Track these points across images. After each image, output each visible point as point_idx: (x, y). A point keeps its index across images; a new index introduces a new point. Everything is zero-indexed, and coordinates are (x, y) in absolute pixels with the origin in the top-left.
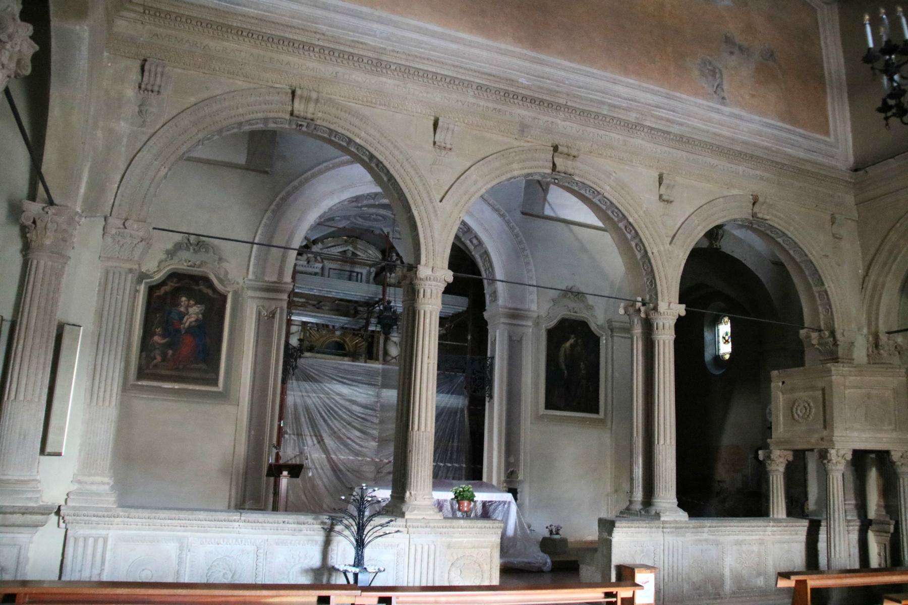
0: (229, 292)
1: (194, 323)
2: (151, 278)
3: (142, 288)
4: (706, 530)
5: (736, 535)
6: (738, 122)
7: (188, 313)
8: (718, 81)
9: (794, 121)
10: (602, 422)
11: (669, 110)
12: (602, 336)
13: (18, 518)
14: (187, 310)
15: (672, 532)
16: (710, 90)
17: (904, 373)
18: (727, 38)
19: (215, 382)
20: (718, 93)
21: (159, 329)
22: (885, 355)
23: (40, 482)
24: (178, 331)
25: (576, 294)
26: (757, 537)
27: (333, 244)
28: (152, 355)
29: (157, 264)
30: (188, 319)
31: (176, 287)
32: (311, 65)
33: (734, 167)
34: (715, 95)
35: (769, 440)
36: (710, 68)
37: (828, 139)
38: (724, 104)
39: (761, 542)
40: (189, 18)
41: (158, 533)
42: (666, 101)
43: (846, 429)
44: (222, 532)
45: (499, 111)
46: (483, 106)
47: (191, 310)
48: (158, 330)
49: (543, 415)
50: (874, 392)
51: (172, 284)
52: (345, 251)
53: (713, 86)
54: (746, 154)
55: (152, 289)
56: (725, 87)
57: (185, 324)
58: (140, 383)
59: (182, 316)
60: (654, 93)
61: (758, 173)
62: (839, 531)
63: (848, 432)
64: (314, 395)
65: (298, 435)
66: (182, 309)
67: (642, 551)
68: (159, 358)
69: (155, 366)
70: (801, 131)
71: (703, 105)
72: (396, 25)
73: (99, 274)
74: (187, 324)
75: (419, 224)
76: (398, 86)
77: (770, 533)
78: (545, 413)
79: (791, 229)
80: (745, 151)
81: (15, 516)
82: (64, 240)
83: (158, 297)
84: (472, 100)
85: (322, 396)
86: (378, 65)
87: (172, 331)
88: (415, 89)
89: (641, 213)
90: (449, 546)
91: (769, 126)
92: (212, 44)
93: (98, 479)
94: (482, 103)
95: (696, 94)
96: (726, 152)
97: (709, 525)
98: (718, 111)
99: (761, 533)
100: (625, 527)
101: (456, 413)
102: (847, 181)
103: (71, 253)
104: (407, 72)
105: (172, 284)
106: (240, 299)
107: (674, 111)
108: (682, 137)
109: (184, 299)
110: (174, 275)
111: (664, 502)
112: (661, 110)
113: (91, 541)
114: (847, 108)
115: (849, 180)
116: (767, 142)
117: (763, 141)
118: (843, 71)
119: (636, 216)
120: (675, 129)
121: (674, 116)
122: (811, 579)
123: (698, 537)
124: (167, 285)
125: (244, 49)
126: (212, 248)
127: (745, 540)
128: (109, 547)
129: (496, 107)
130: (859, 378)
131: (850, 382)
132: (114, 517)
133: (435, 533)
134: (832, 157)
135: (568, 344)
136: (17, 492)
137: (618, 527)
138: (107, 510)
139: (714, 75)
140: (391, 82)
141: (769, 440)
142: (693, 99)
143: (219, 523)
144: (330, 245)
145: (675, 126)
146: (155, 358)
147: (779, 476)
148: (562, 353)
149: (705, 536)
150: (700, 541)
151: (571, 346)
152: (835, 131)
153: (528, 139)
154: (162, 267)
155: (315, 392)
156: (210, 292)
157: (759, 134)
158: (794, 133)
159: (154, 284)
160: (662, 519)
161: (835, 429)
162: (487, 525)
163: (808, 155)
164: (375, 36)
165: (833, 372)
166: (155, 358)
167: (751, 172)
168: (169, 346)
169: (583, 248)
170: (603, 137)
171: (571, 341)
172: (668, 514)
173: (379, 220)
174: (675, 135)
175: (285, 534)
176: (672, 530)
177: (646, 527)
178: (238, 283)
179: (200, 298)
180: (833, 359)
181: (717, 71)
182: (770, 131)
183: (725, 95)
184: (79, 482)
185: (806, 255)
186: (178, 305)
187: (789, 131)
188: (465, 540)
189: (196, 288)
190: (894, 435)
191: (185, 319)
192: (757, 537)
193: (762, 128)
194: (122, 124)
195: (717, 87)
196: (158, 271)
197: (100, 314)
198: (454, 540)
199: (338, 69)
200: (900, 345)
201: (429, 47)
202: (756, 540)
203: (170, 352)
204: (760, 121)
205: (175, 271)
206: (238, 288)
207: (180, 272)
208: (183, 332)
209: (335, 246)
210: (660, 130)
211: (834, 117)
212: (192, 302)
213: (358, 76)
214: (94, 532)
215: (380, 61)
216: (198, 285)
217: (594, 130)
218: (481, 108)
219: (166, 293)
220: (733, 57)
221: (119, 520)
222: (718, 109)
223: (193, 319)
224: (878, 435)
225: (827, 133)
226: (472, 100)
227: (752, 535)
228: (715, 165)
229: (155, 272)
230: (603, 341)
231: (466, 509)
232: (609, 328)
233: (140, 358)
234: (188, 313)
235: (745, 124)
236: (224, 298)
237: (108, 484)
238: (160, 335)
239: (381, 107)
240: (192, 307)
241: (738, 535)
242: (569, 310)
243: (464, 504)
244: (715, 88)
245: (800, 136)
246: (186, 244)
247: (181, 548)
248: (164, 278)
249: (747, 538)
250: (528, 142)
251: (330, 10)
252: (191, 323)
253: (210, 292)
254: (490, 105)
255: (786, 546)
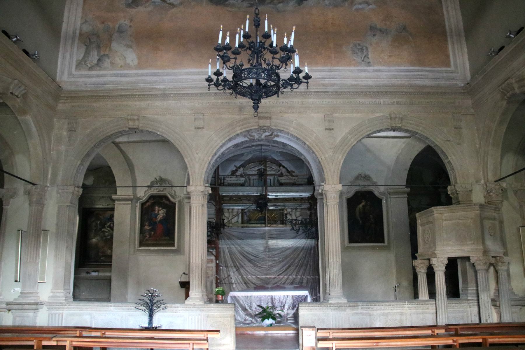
0: (176, 201)
1: (162, 218)
2: (142, 199)
3: (138, 205)
4: (360, 307)
5: (382, 310)
6: (379, 74)
7: (159, 213)
8: (365, 53)
9: (421, 63)
10: (388, 248)
11: (330, 78)
12: (383, 198)
13: (27, 307)
14: (159, 212)
15: (337, 309)
16: (359, 60)
17: (478, 208)
18: (371, 27)
19: (173, 245)
20: (365, 61)
21: (147, 223)
22: (494, 196)
23: (38, 293)
24: (156, 223)
25: (367, 178)
26: (398, 311)
27: (253, 166)
28: (145, 235)
29: (144, 193)
30: (159, 216)
31: (153, 202)
32: (137, 103)
33: (377, 100)
34: (363, 63)
35: (416, 255)
36: (359, 48)
37: (449, 69)
38: (369, 66)
39: (402, 314)
40: (83, 97)
41: (82, 312)
42: (329, 74)
43: (444, 245)
44: (106, 311)
45: (229, 103)
46: (220, 103)
47: (160, 212)
48: (147, 223)
49: (347, 246)
50: (460, 221)
51: (151, 201)
52: (259, 169)
53: (362, 58)
54: (382, 92)
55: (143, 205)
56: (370, 56)
57: (158, 219)
58: (140, 248)
59: (157, 215)
60: (324, 71)
61: (395, 100)
62: (442, 306)
63: (445, 247)
64: (233, 246)
65: (226, 267)
66: (156, 212)
67: (319, 319)
68: (148, 236)
69: (147, 240)
70: (428, 69)
71: (354, 70)
72: (175, 74)
73: (56, 209)
74: (159, 219)
75: (188, 166)
76: (177, 103)
77: (407, 309)
78: (349, 245)
79: (421, 128)
80: (381, 90)
81: (25, 306)
82: (41, 198)
83: (146, 208)
84: (214, 101)
85: (237, 246)
86: (164, 96)
87: (153, 223)
88: (186, 102)
89: (314, 138)
90: (208, 317)
91: (402, 71)
92: (94, 104)
93: (59, 291)
94: (219, 101)
95: (349, 65)
96: (368, 93)
97: (361, 305)
98: (365, 71)
99: (400, 308)
100: (305, 307)
101: (311, 250)
102: (461, 92)
103: (46, 202)
104: (179, 96)
105: (151, 201)
106: (182, 204)
107: (333, 78)
108: (336, 92)
109: (157, 207)
110: (152, 197)
111: (333, 293)
112: (325, 80)
113: (57, 315)
114: (465, 46)
115: (462, 91)
116: (401, 81)
117: (398, 81)
118: (461, 24)
119: (310, 141)
120: (330, 89)
121: (334, 81)
122: (490, 338)
123: (356, 312)
124: (149, 202)
125: (107, 104)
126: (168, 181)
127: (389, 313)
128: (64, 318)
129: (227, 101)
130: (450, 214)
131: (445, 217)
132: (64, 306)
133: (200, 310)
134: (453, 79)
135: (361, 206)
136: (28, 297)
137: (301, 307)
138: (61, 303)
139: (362, 49)
140: (173, 102)
141: (416, 255)
142: (348, 68)
143: (104, 307)
144: (251, 167)
145: (329, 87)
146: (146, 237)
147: (422, 275)
148: (357, 209)
149: (360, 311)
150: (357, 313)
151: (363, 206)
152: (455, 61)
153: (244, 114)
154: (146, 194)
155: (233, 245)
156: (167, 202)
157: (395, 77)
158: (422, 71)
159: (143, 202)
160: (330, 302)
161: (437, 246)
162: (226, 306)
163: (433, 82)
164: (166, 83)
165: (435, 212)
166: (146, 237)
167: (390, 101)
168: (151, 230)
169: (368, 150)
170: (289, 102)
171: (363, 203)
172: (334, 299)
173: (267, 152)
174: (332, 92)
175: (132, 312)
176: (335, 308)
177: (319, 307)
178: (181, 197)
179: (164, 206)
180: (457, 202)
181: (364, 48)
182: (403, 74)
183: (370, 60)
184: (52, 292)
185: (434, 143)
186: (154, 210)
187: (418, 71)
188: (216, 313)
189: (161, 201)
190: (473, 247)
191: (158, 217)
192: (398, 311)
193: (397, 74)
194: (63, 147)
195: (364, 58)
196: (145, 196)
197: (57, 225)
198: (210, 313)
199: (149, 102)
200: (504, 188)
201: (192, 80)
202: (398, 312)
203: (153, 233)
204: (396, 70)
205: (151, 195)
206: (181, 199)
207: (154, 195)
208: (157, 223)
209: (254, 167)
210: (321, 92)
211: (454, 55)
212: (160, 208)
213: (158, 103)
214: (57, 312)
215: (165, 94)
216: (162, 200)
217: (283, 100)
218: (219, 104)
219: (149, 206)
220: (376, 37)
221: (66, 307)
222: (365, 70)
223: (161, 216)
224: (463, 248)
225: (448, 65)
226: (214, 101)
227: (394, 310)
228: (363, 102)
229: (143, 197)
230: (384, 201)
231: (220, 299)
232: (388, 193)
233: (140, 237)
234: (159, 214)
235: (384, 74)
236: (175, 204)
237: (63, 293)
238: (148, 226)
239: (169, 115)
240: (160, 211)
241: (384, 310)
242: (362, 186)
243: (219, 296)
244: (363, 58)
245: (428, 72)
246: (156, 181)
247: (91, 318)
248: (147, 199)
249: (391, 311)
250: (245, 115)
251: (144, 76)
252: (160, 218)
253: (167, 202)
254: (224, 101)
255: (421, 316)
